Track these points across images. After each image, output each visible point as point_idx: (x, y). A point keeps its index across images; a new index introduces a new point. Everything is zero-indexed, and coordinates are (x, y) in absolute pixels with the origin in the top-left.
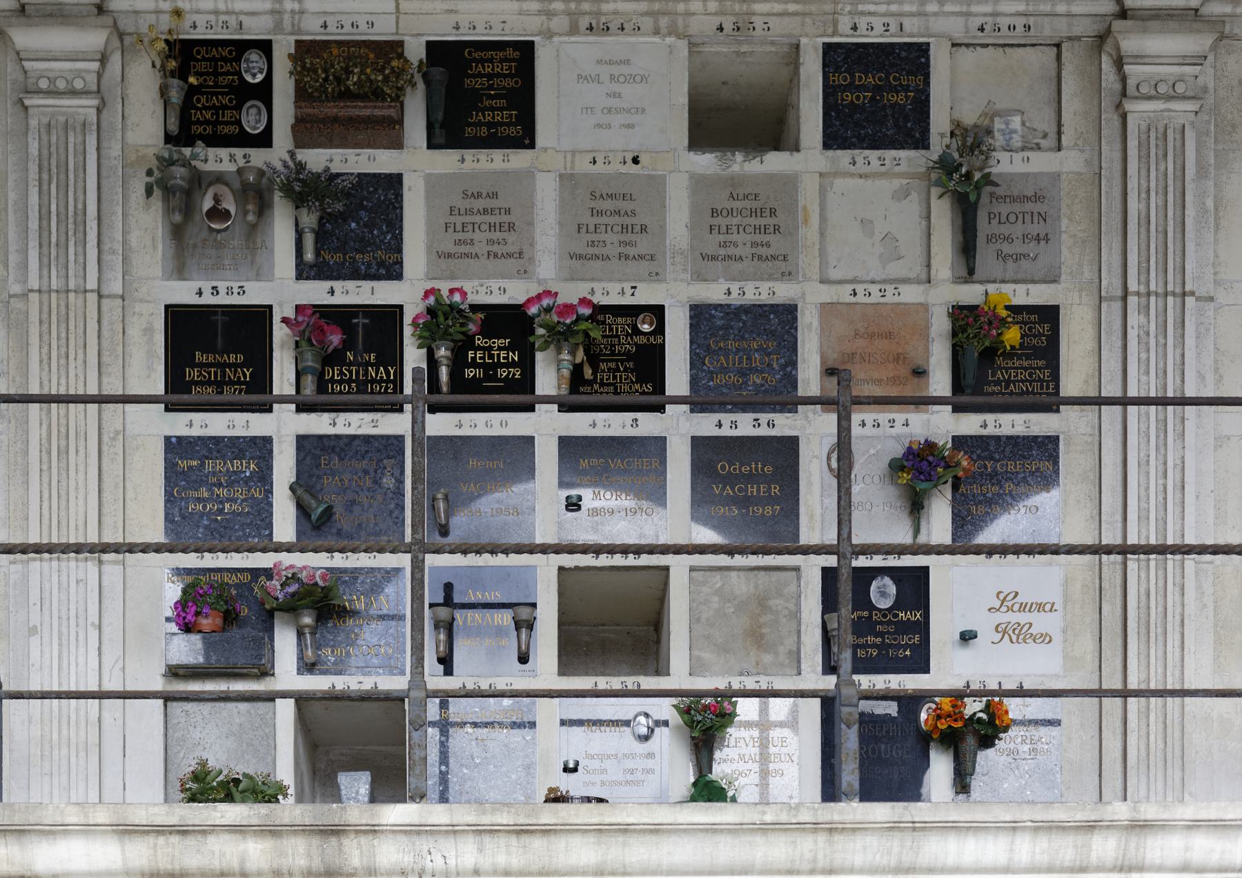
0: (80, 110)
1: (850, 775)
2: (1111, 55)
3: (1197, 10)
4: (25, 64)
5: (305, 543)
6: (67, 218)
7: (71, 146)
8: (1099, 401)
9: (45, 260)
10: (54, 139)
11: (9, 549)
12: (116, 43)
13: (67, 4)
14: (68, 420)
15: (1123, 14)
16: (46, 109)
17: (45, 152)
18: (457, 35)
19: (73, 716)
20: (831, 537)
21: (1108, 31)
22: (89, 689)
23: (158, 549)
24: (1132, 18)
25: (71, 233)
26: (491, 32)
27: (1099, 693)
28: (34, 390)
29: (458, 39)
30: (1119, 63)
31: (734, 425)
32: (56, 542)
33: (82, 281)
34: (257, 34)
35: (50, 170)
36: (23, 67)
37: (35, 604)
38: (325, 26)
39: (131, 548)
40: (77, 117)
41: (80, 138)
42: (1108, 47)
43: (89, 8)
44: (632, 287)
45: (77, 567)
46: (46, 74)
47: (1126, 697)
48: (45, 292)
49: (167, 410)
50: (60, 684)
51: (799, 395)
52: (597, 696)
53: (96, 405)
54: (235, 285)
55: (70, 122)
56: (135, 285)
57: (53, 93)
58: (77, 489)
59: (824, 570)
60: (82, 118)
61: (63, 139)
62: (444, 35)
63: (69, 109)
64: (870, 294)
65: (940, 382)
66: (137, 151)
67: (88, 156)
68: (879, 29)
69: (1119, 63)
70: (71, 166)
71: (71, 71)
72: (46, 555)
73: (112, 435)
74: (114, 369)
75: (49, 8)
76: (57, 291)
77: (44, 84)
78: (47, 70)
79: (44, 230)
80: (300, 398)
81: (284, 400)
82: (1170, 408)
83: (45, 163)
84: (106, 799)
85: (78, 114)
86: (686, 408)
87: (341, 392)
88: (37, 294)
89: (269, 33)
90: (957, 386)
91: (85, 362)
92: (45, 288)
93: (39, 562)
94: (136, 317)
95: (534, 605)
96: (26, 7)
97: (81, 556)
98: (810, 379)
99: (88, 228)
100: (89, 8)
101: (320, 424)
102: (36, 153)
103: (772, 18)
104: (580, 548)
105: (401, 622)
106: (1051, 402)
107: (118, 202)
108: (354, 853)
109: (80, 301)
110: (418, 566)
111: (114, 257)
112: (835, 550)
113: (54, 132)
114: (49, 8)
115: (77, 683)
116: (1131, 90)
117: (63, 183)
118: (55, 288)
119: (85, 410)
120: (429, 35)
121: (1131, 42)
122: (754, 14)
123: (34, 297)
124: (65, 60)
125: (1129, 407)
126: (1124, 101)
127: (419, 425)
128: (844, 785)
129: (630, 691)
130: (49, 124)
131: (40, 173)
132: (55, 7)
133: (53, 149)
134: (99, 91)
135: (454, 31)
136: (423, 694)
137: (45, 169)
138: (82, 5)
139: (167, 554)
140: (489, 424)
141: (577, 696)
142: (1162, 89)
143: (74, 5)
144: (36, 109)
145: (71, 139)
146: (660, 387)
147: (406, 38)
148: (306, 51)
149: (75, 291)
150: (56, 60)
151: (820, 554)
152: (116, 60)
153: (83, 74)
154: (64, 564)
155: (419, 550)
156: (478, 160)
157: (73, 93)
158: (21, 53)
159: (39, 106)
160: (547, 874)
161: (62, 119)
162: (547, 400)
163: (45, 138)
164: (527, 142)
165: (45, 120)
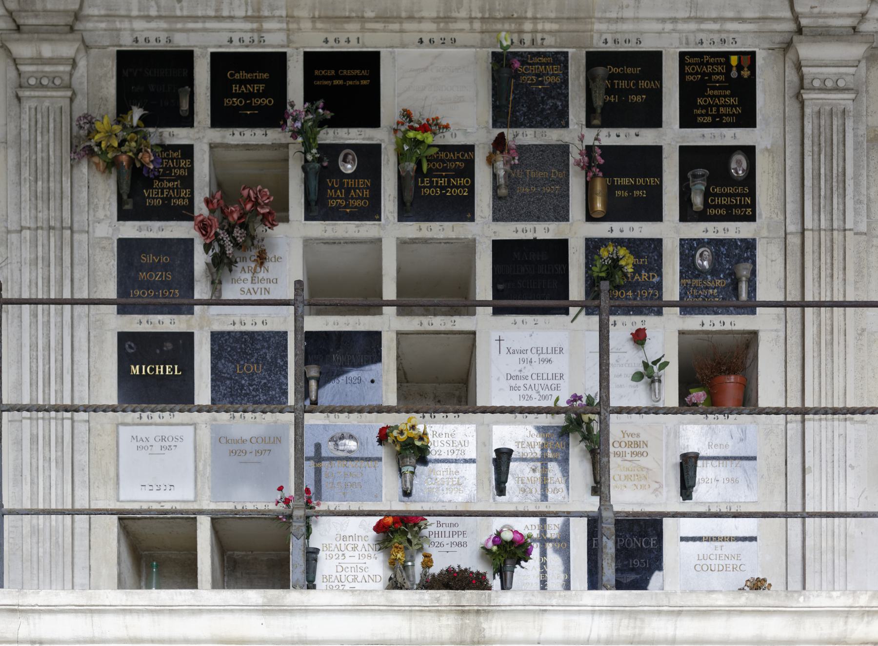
0: (841, 102)
1: (609, 571)
2: (790, 59)
3: (854, 28)
4: (20, 67)
6: (832, 178)
7: (835, 127)
9: (816, 208)
10: (822, 122)
11: (874, 411)
12: (82, 47)
13: (833, 27)
14: (832, 321)
15: (800, 31)
16: (818, 101)
17: (816, 131)
18: (137, 47)
19: (836, 531)
22: (848, 511)
23: (114, 410)
25: (834, 189)
26: (149, 44)
27: (787, 515)
28: (25, 296)
29: (616, 50)
32: (811, 406)
33: (842, 223)
34: (371, 47)
35: (820, 144)
36: (18, 69)
37: (809, 452)
38: (326, 41)
39: (96, 409)
40: (839, 107)
41: (840, 122)
42: (790, 55)
43: (848, 29)
45: (56, 423)
46: (817, 76)
47: (804, 518)
48: (815, 230)
49: (120, 312)
50: (827, 508)
52: (720, 517)
53: (70, 306)
55: (834, 110)
56: (873, 225)
57: (824, 89)
58: (839, 370)
60: (843, 107)
61: (828, 122)
63: (834, 101)
65: (672, 288)
66: (875, 130)
67: (847, 134)
68: (353, 41)
69: (798, 67)
70: (835, 142)
71: (835, 74)
72: (830, 416)
73: (859, 332)
74: (837, 283)
75: (820, 30)
76: (825, 230)
77: (32, 81)
78: (818, 73)
79: (817, 186)
80: (682, 303)
82: (40, 307)
83: (816, 139)
85: (840, 104)
86: (114, 308)
87: (139, 297)
89: (282, 46)
90: (497, 293)
91: (845, 280)
94: (874, 248)
96: (21, 27)
99: (847, 185)
100: (848, 29)
102: (810, 132)
104: (499, 410)
106: (750, 307)
107: (863, 166)
108: (493, 627)
109: (841, 237)
110: (299, 425)
111: (861, 206)
113: (822, 117)
114: (820, 30)
115: (839, 508)
116: (806, 82)
117: (829, 153)
118: (824, 228)
119: (845, 315)
120: (305, 47)
121: (806, 51)
124: (833, 66)
125: (806, 309)
126: (802, 91)
127: (298, 319)
128: (605, 579)
130: (819, 112)
131: (813, 146)
132: (824, 29)
133: (822, 129)
135: (324, 44)
137: (816, 144)
138: (843, 27)
141: (455, 516)
142: (829, 84)
143: (838, 27)
144: (810, 102)
145: (835, 123)
148: (594, 59)
149: (838, 230)
150: (826, 66)
153: (844, 76)
154: (823, 423)
155: (299, 413)
156: (255, 134)
157: (837, 89)
158: (17, 60)
159: (812, 99)
160: (639, 643)
161: (828, 108)
162: (390, 304)
163: (816, 121)
164: (282, 123)
165: (816, 109)
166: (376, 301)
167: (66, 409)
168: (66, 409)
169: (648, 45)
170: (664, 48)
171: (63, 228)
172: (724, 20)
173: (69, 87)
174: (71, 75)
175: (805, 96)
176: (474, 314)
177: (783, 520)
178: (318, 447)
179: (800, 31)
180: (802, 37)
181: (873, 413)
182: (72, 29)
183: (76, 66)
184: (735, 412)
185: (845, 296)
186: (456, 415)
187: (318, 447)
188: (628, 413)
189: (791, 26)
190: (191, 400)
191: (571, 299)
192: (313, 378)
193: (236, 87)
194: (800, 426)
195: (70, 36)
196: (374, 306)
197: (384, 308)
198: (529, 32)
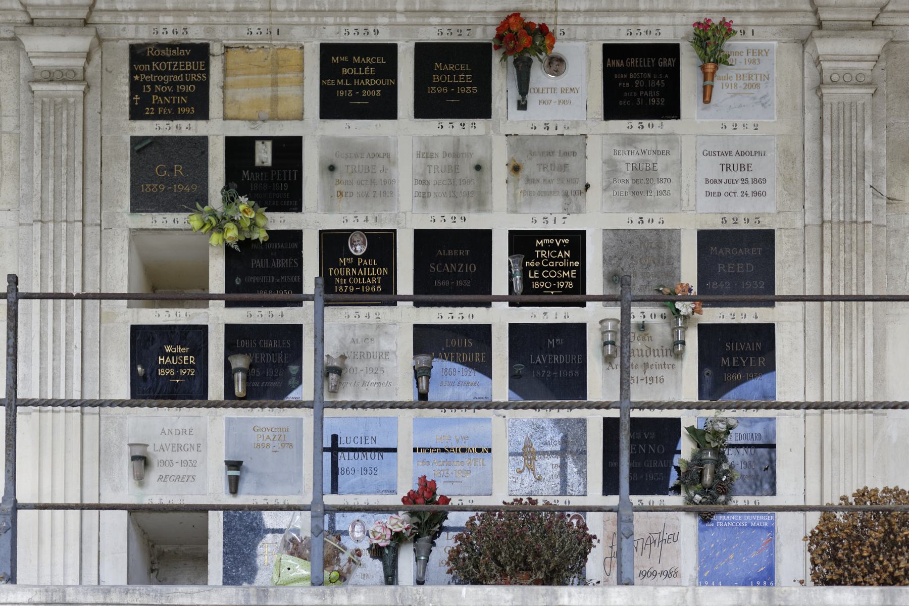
3: (873, 22)
5: (136, 402)
8: (83, 297)
11: (905, 406)
20: (615, 397)
21: (811, 36)
24: (39, 26)
28: (869, 292)
30: (817, 62)
31: (733, 316)
39: (886, 406)
42: (808, 48)
44: (564, 218)
49: (510, 305)
51: (210, 293)
54: (638, 215)
59: (607, 421)
62: (387, 41)
64: (632, 222)
65: (405, 283)
69: (817, 62)
81: (500, 299)
84: (84, 583)
86: (411, 303)
88: (65, 223)
90: (417, 289)
92: (847, 220)
93: (38, 413)
95: (773, 447)
96: (34, 20)
97: (847, 410)
98: (595, 283)
101: (241, 316)
103: (662, 27)
104: (595, 405)
105: (582, 456)
112: (618, 405)
121: (825, 46)
122: (638, 25)
123: (869, 229)
129: (751, 507)
134: (84, 79)
136: (313, 509)
139: (128, 408)
140: (744, 316)
146: (488, 289)
147: (210, 42)
151: (423, 408)
152: (96, 58)
155: (317, 406)
162: (405, 298)
166: (771, 297)
167: (72, 403)
168: (72, 403)
169: (384, 37)
170: (210, 40)
171: (823, 222)
172: (637, 11)
173: (84, 79)
174: (84, 70)
175: (824, 91)
176: (207, 306)
177: (78, 511)
178: (335, 438)
179: (820, 25)
180: (823, 33)
181: (904, 408)
182: (86, 23)
183: (90, 60)
184: (901, 406)
185: (100, 290)
186: (271, 409)
187: (335, 438)
188: (343, 407)
189: (810, 20)
190: (584, 396)
191: (493, 293)
192: (237, 370)
193: (357, 81)
194: (819, 418)
195: (86, 30)
196: (203, 298)
197: (211, 302)
198: (331, 25)
